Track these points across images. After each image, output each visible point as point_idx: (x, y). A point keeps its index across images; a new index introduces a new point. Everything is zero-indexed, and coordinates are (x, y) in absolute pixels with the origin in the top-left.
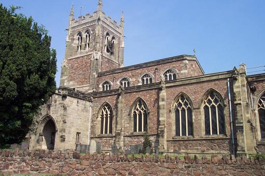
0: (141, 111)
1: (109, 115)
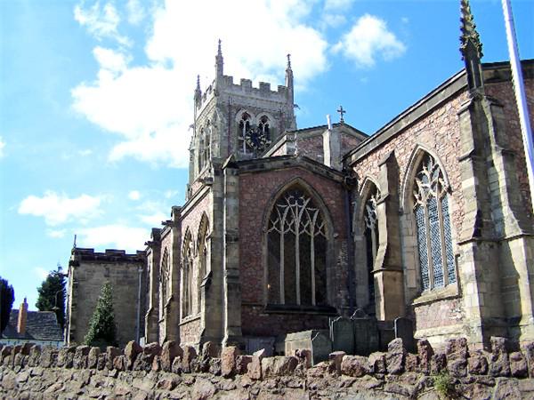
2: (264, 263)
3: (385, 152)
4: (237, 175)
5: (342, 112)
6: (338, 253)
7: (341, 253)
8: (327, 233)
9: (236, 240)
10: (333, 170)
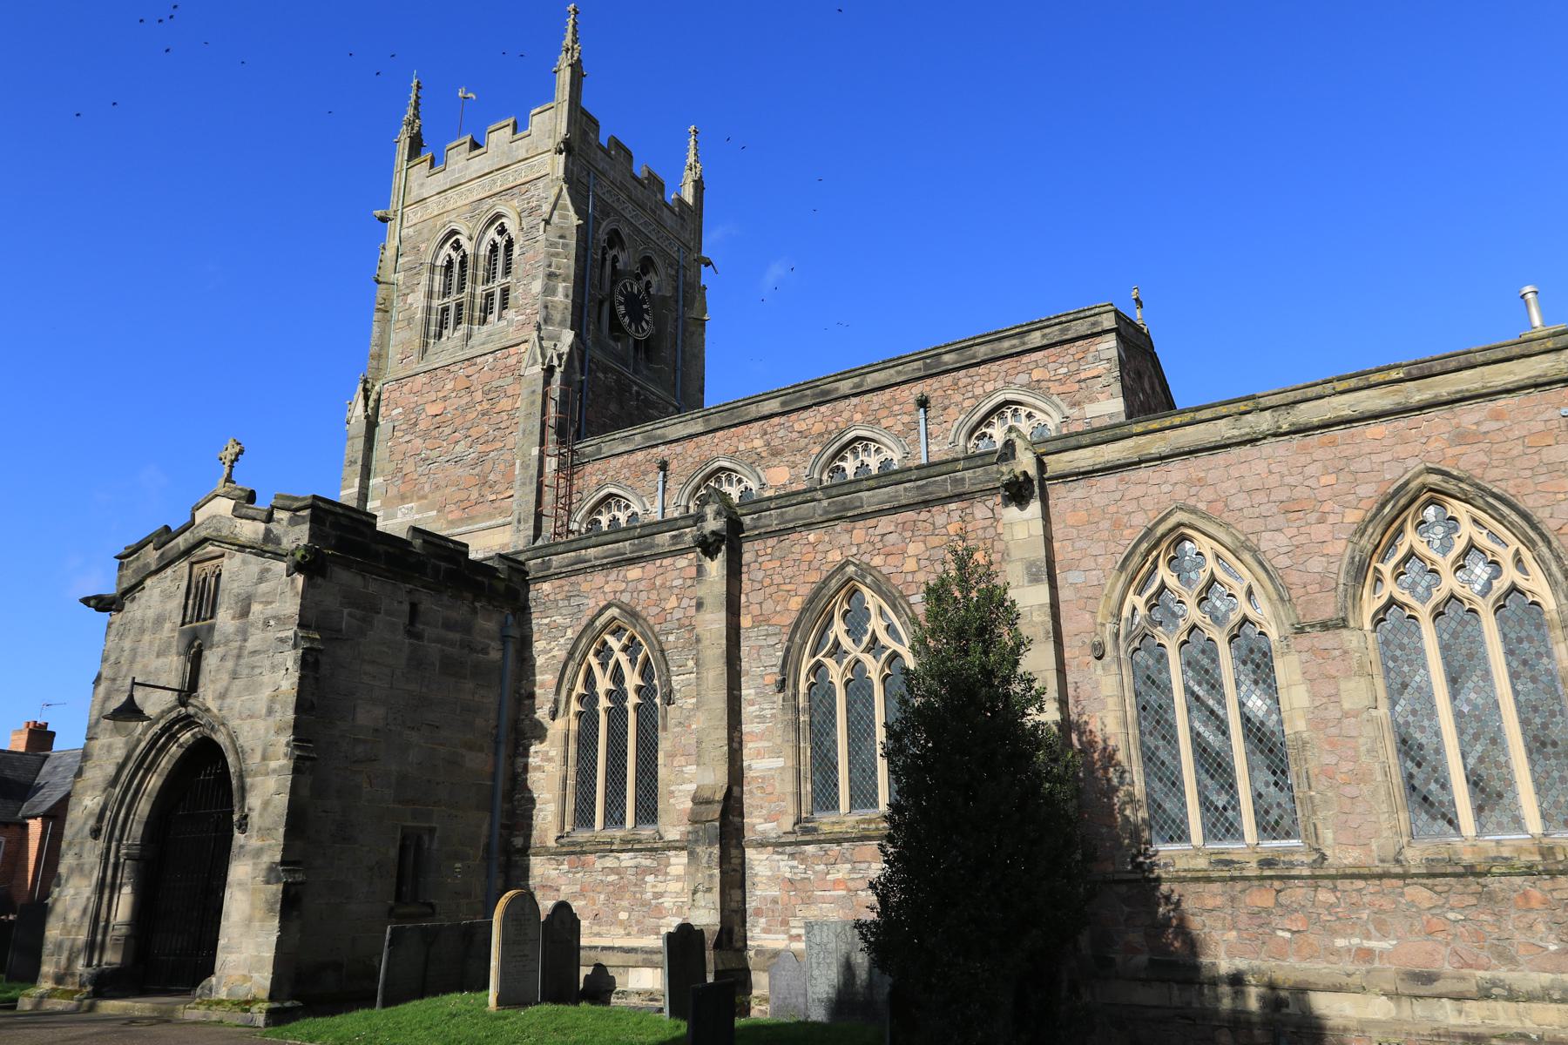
0: (867, 659)
1: (633, 699)
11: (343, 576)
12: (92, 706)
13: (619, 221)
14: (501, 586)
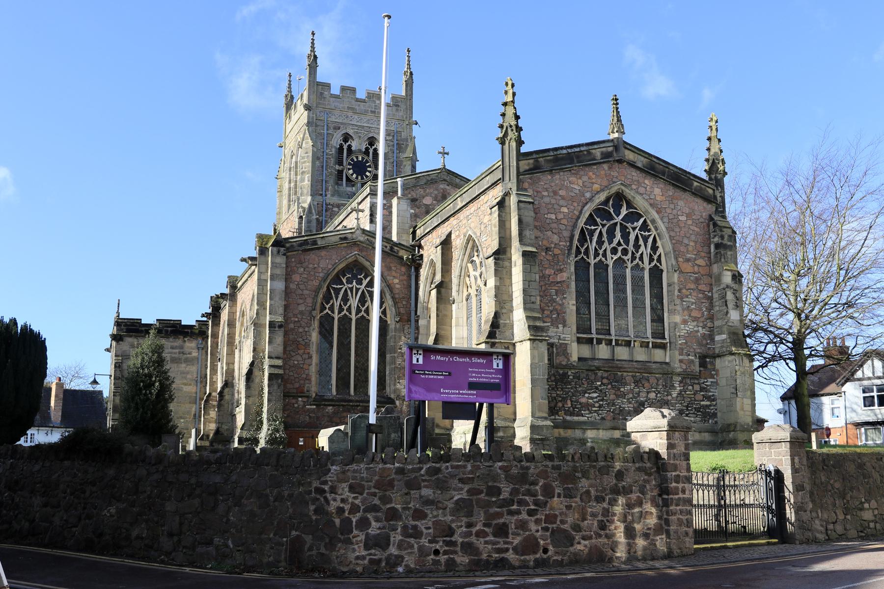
2: (313, 350)
3: (443, 231)
4: (284, 254)
5: (444, 153)
6: (400, 338)
7: (403, 338)
8: (388, 316)
9: (280, 326)
10: (399, 245)
11: (129, 340)
12: (111, 381)
13: (346, 128)
14: (197, 331)
